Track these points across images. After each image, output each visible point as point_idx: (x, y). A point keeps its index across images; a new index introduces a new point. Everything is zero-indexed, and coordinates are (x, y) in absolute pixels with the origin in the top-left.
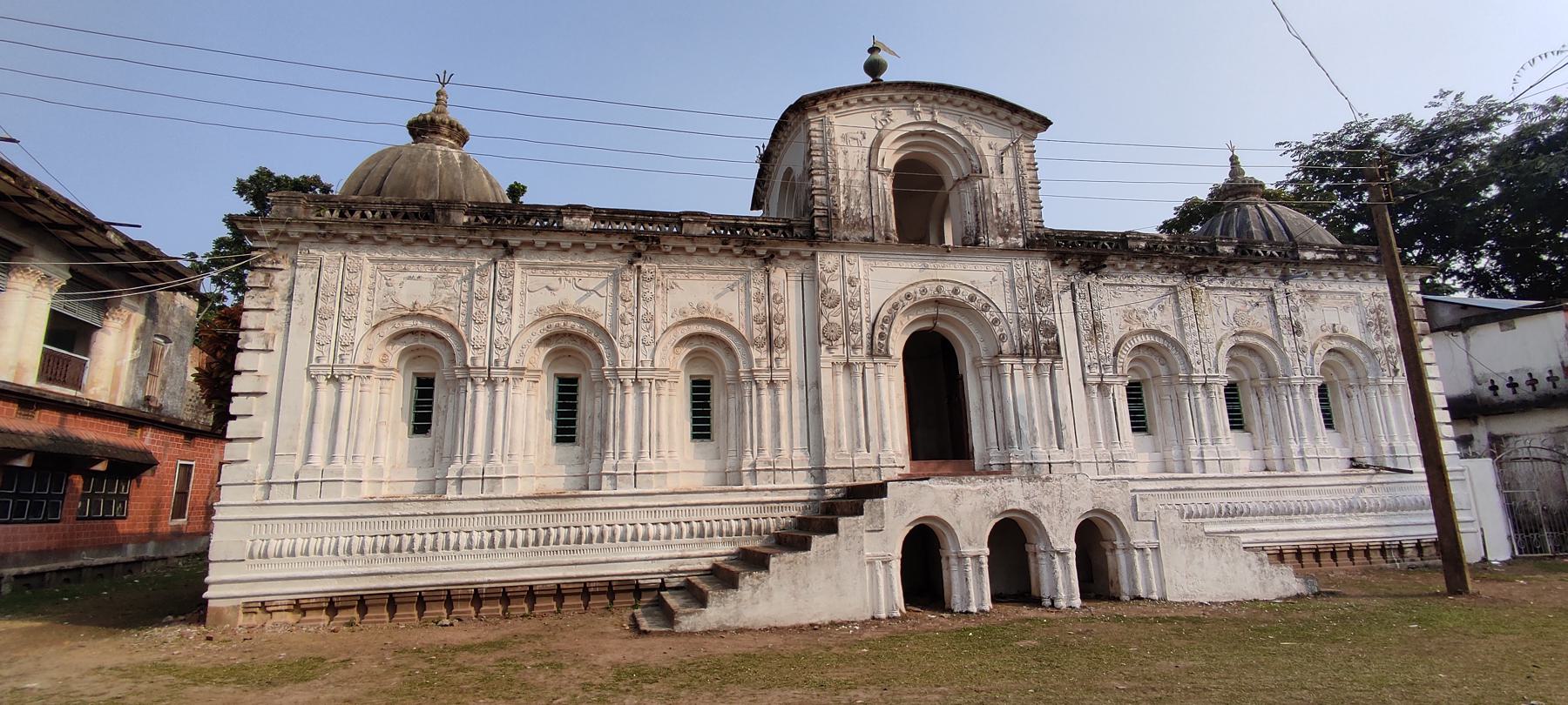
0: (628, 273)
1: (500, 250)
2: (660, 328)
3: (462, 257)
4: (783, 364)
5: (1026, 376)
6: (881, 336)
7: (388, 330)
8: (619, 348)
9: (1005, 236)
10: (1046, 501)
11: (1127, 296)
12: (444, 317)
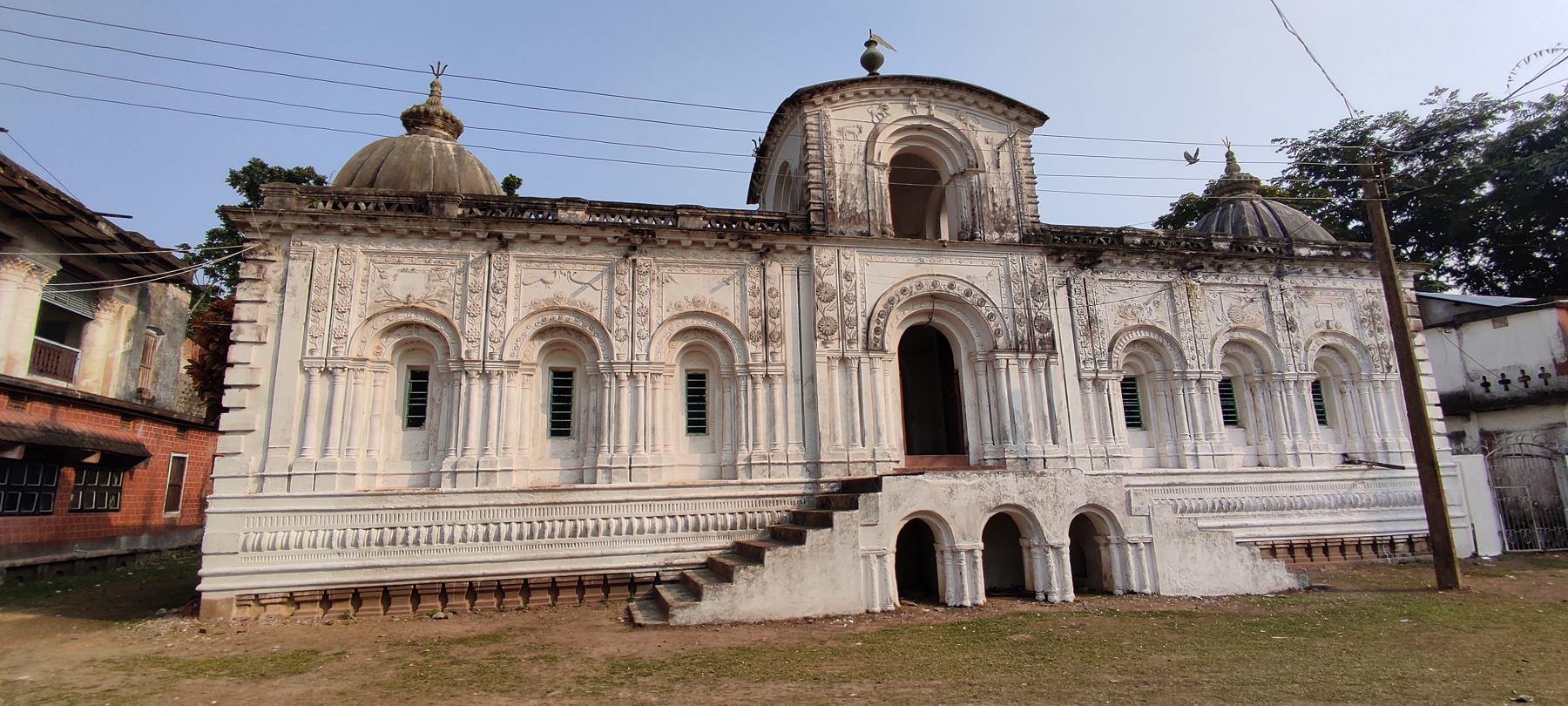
0: (623, 266)
1: (495, 243)
2: (655, 321)
3: (456, 250)
4: (778, 358)
6: (877, 331)
7: (382, 323)
9: (1001, 231)
10: (1040, 496)
11: (1122, 291)
12: (438, 309)
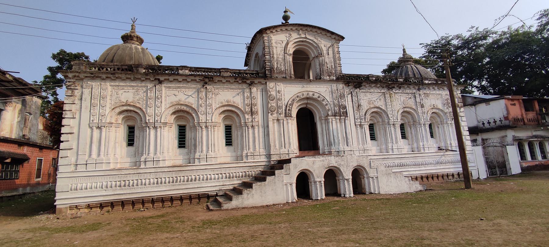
0: (202, 89)
1: (157, 82)
2: (214, 108)
3: (143, 84)
4: (256, 120)
5: (336, 122)
6: (289, 110)
7: (118, 110)
8: (200, 115)
9: (329, 76)
12: (138, 105)
